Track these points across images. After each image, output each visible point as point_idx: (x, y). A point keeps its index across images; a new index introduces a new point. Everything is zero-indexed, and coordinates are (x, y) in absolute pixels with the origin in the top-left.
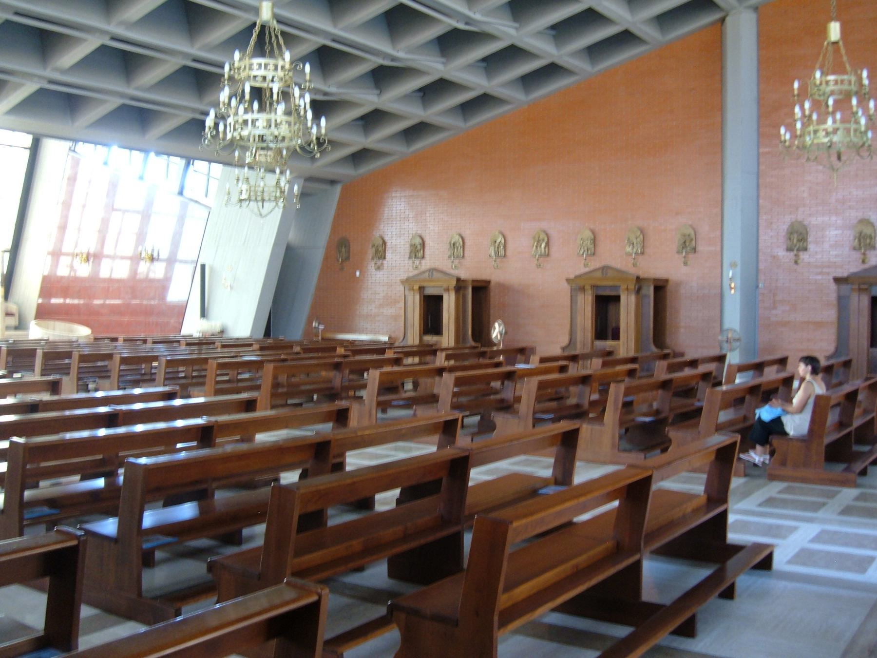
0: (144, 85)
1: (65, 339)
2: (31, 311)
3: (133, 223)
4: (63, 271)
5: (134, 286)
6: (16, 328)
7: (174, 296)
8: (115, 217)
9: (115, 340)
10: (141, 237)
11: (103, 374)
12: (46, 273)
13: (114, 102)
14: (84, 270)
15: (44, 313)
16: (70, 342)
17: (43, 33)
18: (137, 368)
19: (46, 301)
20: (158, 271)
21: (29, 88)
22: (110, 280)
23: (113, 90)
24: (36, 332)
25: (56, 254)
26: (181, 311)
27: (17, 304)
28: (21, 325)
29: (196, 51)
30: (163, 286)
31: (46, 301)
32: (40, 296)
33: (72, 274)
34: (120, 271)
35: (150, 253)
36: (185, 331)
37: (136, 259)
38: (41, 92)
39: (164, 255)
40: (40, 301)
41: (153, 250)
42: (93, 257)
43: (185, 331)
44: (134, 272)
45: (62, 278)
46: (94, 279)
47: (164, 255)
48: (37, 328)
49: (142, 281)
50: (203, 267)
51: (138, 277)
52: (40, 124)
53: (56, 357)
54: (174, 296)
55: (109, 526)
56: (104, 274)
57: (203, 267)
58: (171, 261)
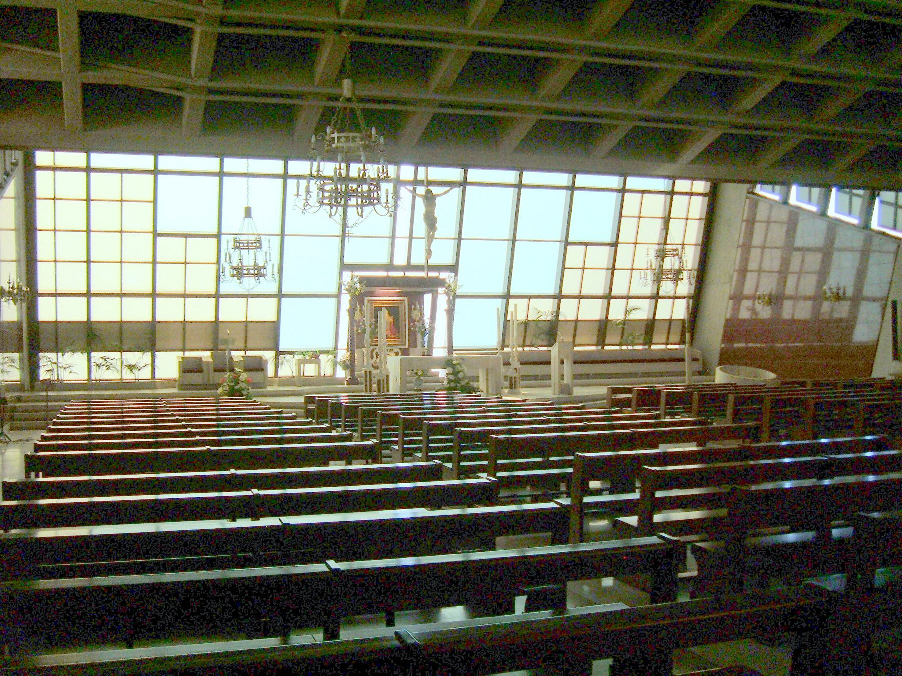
0: (826, 119)
1: (751, 383)
2: (715, 356)
3: (814, 261)
4: (744, 315)
5: (818, 327)
6: (700, 373)
7: (862, 334)
8: (796, 258)
9: (803, 384)
10: (823, 274)
11: (794, 420)
12: (728, 317)
13: (624, 127)
14: (765, 313)
15: (727, 358)
16: (754, 387)
17: (624, 71)
18: (830, 414)
19: (728, 345)
20: (843, 310)
21: (710, 136)
22: (793, 321)
23: (798, 126)
24: (720, 376)
25: (737, 298)
26: (869, 351)
27: (700, 349)
28: (705, 370)
29: (881, 74)
30: (849, 325)
31: (728, 345)
32: (723, 341)
33: (754, 317)
34: (803, 312)
35: (835, 291)
36: (876, 374)
37: (818, 298)
38: (724, 138)
39: (850, 293)
40: (723, 345)
41: (839, 289)
42: (775, 300)
43: (876, 374)
44: (816, 311)
45: (744, 321)
46: (776, 320)
47: (850, 293)
48: (722, 373)
49: (828, 322)
50: (894, 304)
51: (821, 318)
52: (721, 170)
53: (747, 399)
54: (862, 334)
55: (834, 582)
56: (786, 314)
57: (894, 304)
58: (857, 300)
